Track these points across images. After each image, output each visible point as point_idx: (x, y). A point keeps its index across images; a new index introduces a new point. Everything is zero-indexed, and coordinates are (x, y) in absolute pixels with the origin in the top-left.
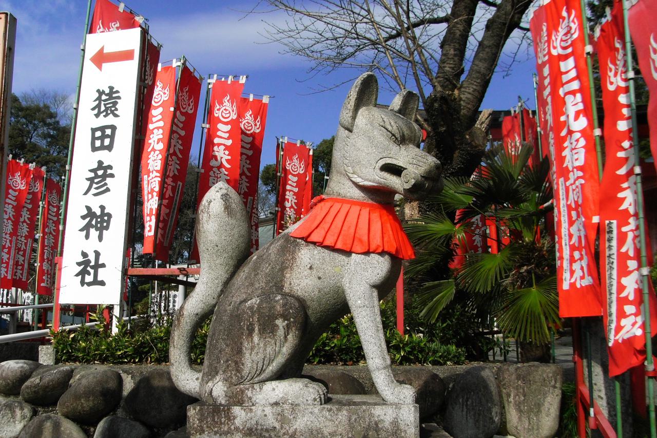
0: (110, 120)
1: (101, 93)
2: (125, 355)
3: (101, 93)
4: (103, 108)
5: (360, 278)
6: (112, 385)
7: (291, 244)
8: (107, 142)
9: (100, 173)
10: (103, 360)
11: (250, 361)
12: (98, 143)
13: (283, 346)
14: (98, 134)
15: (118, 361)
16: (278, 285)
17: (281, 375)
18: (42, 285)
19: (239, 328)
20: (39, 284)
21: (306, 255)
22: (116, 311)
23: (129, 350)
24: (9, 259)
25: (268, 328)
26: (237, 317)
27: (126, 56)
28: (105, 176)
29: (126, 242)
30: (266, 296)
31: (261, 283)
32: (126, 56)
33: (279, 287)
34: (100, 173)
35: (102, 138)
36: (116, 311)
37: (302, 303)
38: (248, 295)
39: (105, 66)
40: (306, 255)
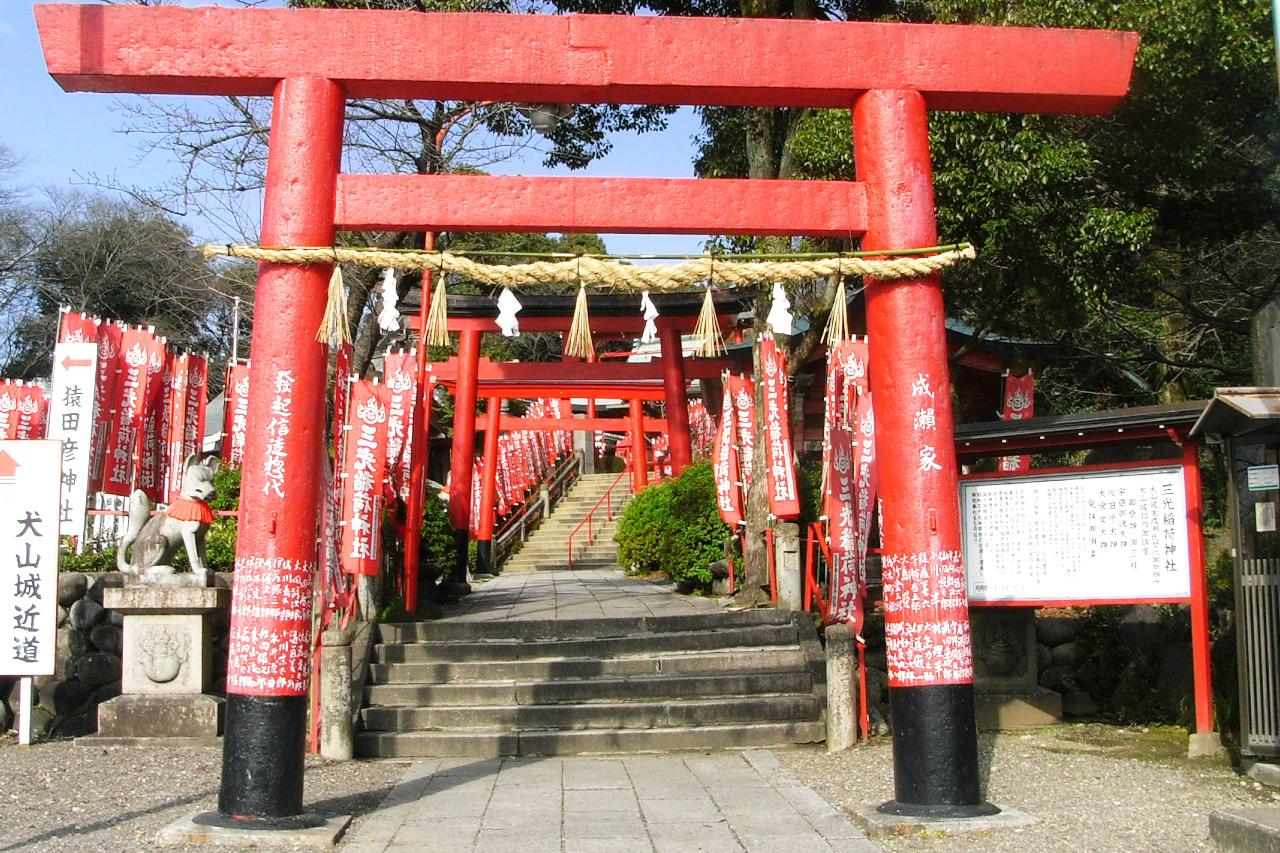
0: (75, 409)
1: (68, 389)
2: (87, 566)
3: (68, 389)
4: (70, 400)
5: (187, 530)
6: (81, 582)
7: (163, 516)
8: (73, 424)
9: (69, 446)
10: (72, 570)
11: (147, 558)
12: (67, 425)
13: (158, 553)
14: (67, 418)
15: (82, 569)
16: (158, 532)
17: (159, 563)
18: (112, 479)
19: (143, 548)
20: (108, 479)
21: (169, 521)
22: (80, 539)
23: (90, 564)
24: (370, 529)
25: (153, 547)
26: (142, 543)
27: (87, 363)
28: (72, 448)
29: (1119, 461)
30: (153, 536)
31: (152, 531)
32: (87, 363)
33: (158, 533)
34: (69, 446)
35: (70, 421)
36: (80, 539)
37: (167, 539)
38: (147, 536)
39: (71, 368)
40: (169, 521)
